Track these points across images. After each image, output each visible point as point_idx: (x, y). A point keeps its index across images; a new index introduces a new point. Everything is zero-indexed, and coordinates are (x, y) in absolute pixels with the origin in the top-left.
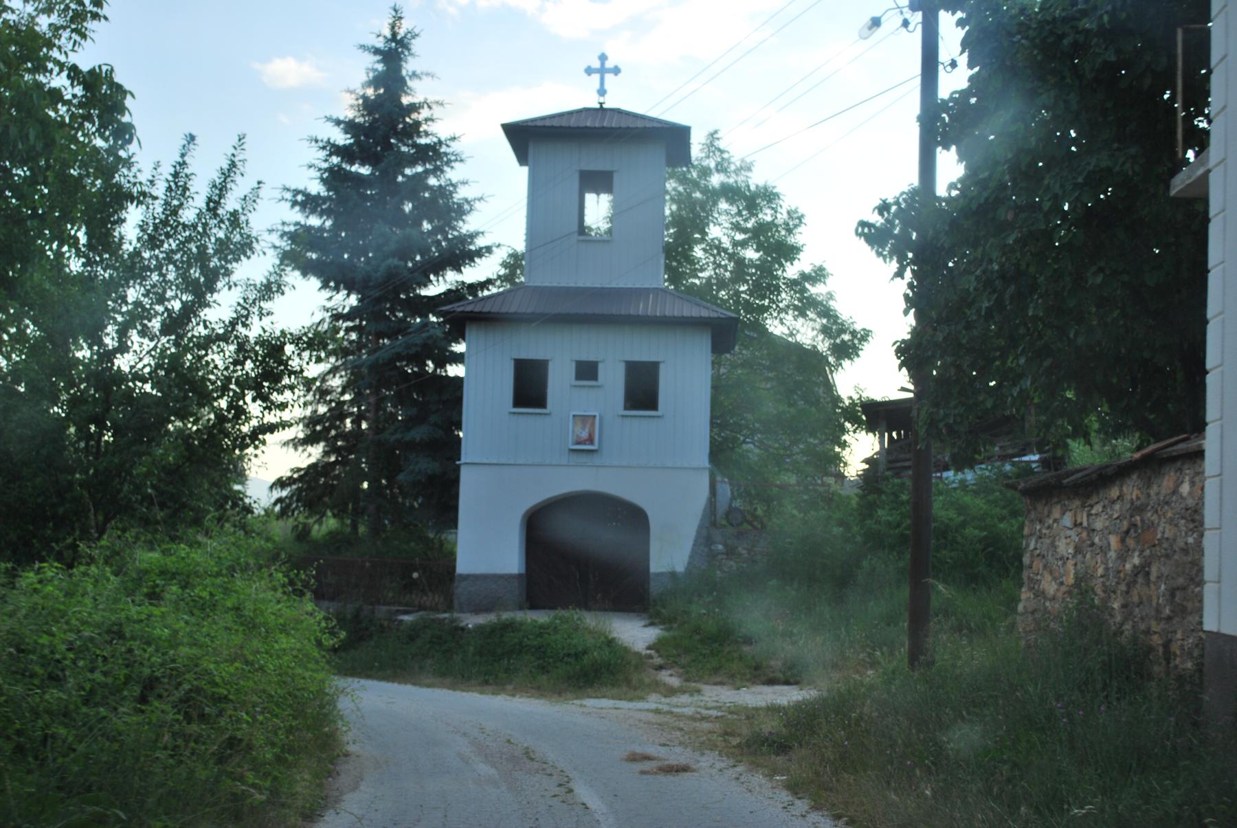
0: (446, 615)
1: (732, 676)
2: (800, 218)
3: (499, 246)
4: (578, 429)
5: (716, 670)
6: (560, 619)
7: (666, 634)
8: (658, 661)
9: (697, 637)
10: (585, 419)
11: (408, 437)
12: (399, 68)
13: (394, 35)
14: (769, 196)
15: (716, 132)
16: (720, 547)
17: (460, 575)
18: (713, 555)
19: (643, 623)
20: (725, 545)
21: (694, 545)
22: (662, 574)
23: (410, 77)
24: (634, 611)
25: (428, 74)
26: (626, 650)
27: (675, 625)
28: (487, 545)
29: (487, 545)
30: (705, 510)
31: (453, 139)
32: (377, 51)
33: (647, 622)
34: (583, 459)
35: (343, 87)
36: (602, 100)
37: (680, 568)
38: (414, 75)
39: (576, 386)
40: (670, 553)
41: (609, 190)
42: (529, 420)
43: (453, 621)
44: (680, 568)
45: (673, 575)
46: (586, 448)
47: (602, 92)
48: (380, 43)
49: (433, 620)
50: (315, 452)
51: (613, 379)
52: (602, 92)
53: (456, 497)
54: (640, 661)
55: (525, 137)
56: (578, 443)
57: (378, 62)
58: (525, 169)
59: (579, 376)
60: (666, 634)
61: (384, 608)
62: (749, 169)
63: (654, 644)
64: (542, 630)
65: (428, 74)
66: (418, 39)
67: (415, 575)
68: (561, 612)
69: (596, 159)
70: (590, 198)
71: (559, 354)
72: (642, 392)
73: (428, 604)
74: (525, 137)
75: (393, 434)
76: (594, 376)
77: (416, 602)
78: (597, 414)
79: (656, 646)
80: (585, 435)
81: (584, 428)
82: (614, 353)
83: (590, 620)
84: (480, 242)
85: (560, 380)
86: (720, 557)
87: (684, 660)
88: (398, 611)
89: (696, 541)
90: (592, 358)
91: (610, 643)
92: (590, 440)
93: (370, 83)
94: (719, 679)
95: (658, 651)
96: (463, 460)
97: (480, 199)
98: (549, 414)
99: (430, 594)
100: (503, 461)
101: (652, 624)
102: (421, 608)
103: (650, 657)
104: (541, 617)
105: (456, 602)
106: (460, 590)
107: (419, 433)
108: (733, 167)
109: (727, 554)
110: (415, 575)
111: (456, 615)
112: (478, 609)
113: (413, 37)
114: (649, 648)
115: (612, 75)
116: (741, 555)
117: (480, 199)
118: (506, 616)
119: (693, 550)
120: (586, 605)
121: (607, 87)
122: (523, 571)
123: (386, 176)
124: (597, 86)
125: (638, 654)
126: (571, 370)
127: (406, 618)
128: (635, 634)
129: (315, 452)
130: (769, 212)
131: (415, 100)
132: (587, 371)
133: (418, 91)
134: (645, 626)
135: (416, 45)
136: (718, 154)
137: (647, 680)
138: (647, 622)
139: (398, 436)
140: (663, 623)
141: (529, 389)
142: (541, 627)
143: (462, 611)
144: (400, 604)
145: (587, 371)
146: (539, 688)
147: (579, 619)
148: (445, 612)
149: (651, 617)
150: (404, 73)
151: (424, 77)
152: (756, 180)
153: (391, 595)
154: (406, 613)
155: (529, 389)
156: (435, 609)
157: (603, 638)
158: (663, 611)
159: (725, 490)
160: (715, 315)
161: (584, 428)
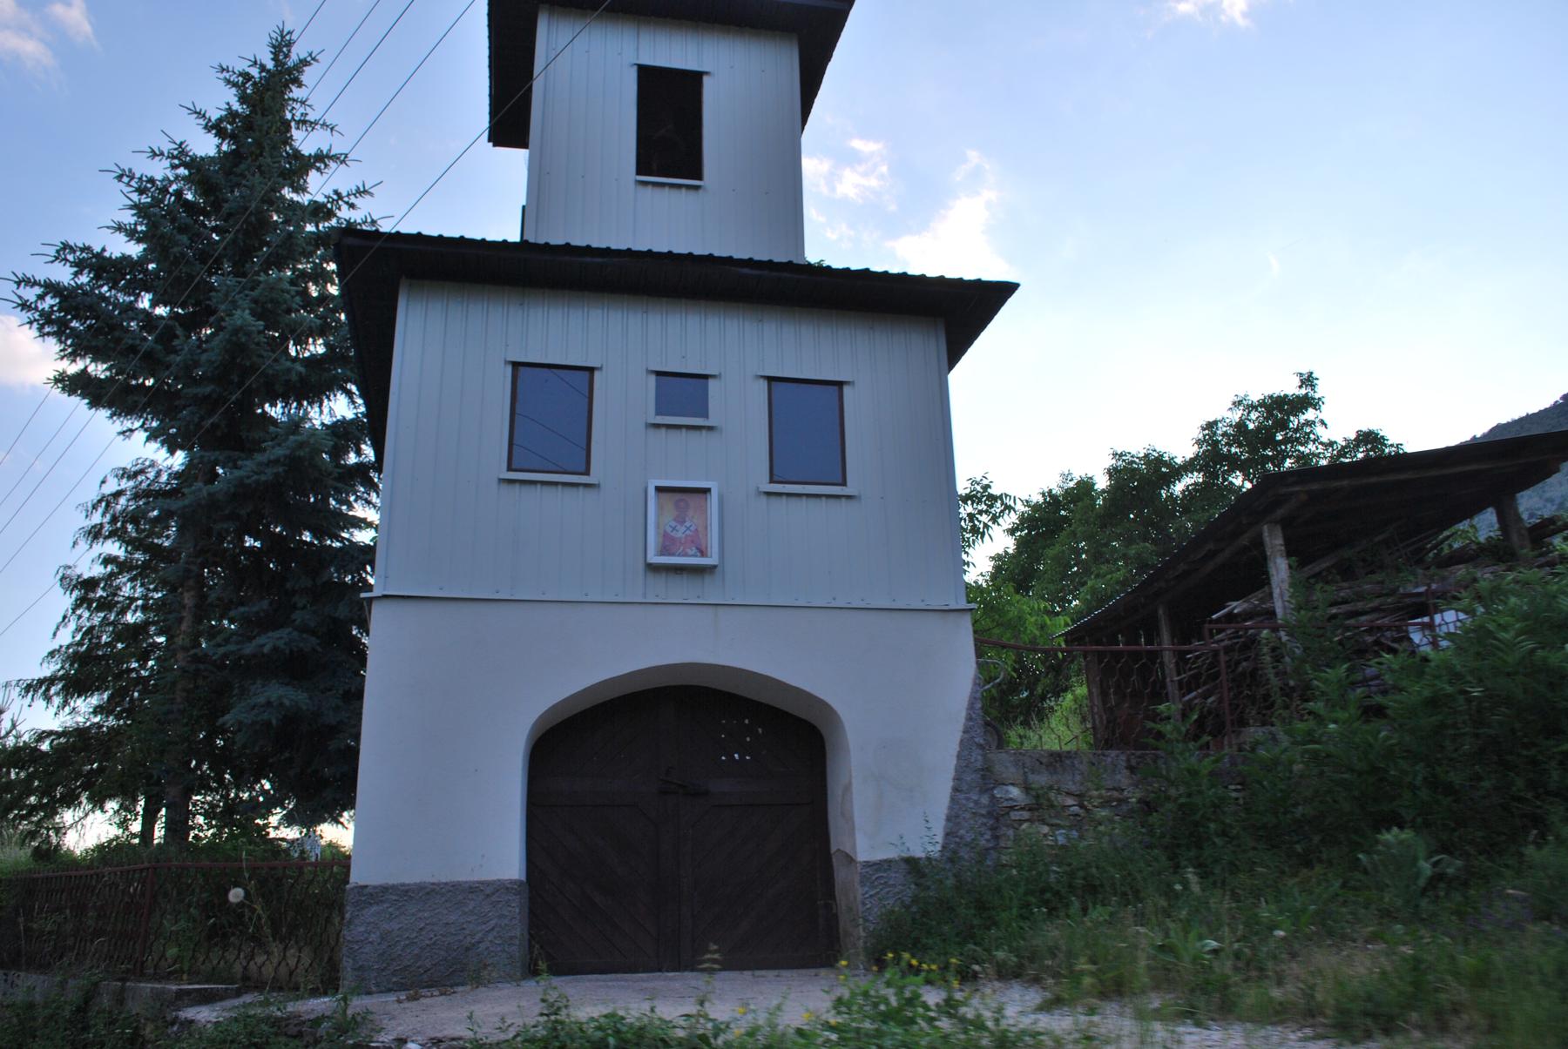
0: (321, 1005)
16: (1015, 792)
18: (998, 815)
20: (1027, 789)
21: (956, 789)
23: (298, 122)
25: (324, 125)
30: (971, 707)
31: (361, 192)
34: (680, 589)
35: (181, 120)
39: (657, 426)
42: (549, 508)
49: (275, 1022)
50: (83, 710)
51: (740, 407)
53: (360, 719)
73: (268, 971)
77: (238, 968)
85: (623, 402)
88: (180, 994)
99: (276, 948)
102: (250, 983)
105: (347, 964)
106: (361, 932)
110: (236, 895)
111: (358, 1004)
122: (523, 878)
127: (204, 1015)
129: (83, 710)
132: (682, 393)
135: (308, 76)
139: (232, 647)
144: (194, 975)
148: (315, 993)
153: (172, 952)
154: (206, 998)
156: (290, 986)
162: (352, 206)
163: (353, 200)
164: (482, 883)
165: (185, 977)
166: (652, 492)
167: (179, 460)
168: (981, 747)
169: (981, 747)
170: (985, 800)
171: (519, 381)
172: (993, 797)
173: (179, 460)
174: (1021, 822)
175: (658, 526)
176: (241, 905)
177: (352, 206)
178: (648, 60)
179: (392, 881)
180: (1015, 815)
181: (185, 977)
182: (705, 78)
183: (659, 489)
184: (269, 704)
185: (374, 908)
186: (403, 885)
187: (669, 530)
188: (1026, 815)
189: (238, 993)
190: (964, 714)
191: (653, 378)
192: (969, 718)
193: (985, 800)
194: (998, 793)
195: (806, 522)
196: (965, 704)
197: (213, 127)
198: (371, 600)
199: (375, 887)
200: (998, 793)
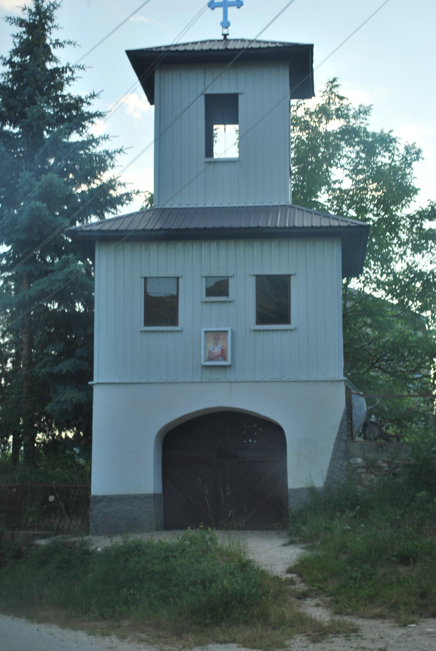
0: (77, 539)
1: (394, 607)
2: (418, 152)
3: (138, 192)
4: (210, 345)
5: (371, 599)
6: (190, 539)
7: (308, 553)
8: (301, 587)
9: (345, 557)
10: (217, 335)
11: (56, 370)
12: (44, 37)
13: (38, 7)
14: (385, 141)
15: (335, 80)
16: (360, 460)
17: (96, 497)
19: (282, 542)
20: (365, 458)
21: (332, 459)
22: (301, 490)
23: (54, 45)
24: (272, 529)
25: (70, 43)
26: (263, 574)
27: (318, 544)
28: (122, 463)
29: (122, 463)
30: (342, 423)
32: (21, 22)
33: (287, 540)
34: (216, 375)
36: (225, 32)
37: (319, 483)
38: (57, 43)
39: (206, 302)
40: (306, 469)
41: (235, 122)
42: (162, 339)
43: (85, 543)
44: (319, 483)
45: (312, 490)
46: (218, 366)
47: (226, 24)
48: (26, 16)
51: (244, 296)
52: (226, 24)
54: (278, 589)
55: (149, 65)
56: (210, 359)
57: (24, 32)
58: (153, 107)
59: (210, 292)
60: (308, 553)
61: (22, 533)
62: (365, 112)
63: (296, 566)
64: (168, 554)
65: (70, 43)
66: (59, 9)
67: (51, 498)
68: (190, 532)
69: (223, 83)
70: (219, 129)
71: (187, 269)
72: (274, 303)
74: (149, 65)
75: (41, 368)
76: (226, 293)
78: (229, 329)
79: (299, 569)
80: (217, 351)
81: (216, 344)
82: (244, 266)
83: (223, 540)
84: (120, 191)
86: (359, 470)
87: (332, 586)
89: (334, 454)
90: (222, 273)
91: (245, 566)
92: (223, 355)
93: (15, 52)
94: (377, 611)
95: (300, 575)
96: (96, 380)
97: (120, 151)
98: (181, 331)
100: (136, 381)
101: (292, 543)
102: (59, 531)
103: (292, 582)
104: (170, 538)
106: (96, 511)
107: (65, 366)
108: (351, 113)
109: (367, 467)
112: (112, 531)
113: (55, 8)
114: (289, 571)
115: (235, 8)
116: (381, 468)
117: (120, 151)
118: (133, 538)
119: (331, 464)
120: (220, 522)
121: (230, 19)
122: (160, 491)
123: (32, 132)
124: (221, 19)
125: (277, 579)
126: (201, 288)
127: (42, 542)
128: (272, 554)
130: (387, 154)
131: (60, 66)
133: (62, 57)
134: (285, 545)
135: (56, 13)
136: (337, 100)
137: (289, 616)
138: (287, 540)
139: (48, 369)
140: (305, 542)
141: (161, 311)
142: (169, 549)
143: (97, 533)
145: (218, 289)
146: (157, 626)
147: (211, 539)
149: (290, 535)
150: (48, 42)
151: (66, 45)
152: (374, 125)
153: (31, 519)
154: (44, 537)
155: (161, 311)
157: (236, 560)
158: (304, 528)
159: (361, 405)
160: (345, 224)
161: (216, 344)
162: (89, 104)
163: (88, 100)
164: (139, 495)
165: (36, 529)
166: (203, 333)
167: (10, 247)
168: (345, 441)
169: (345, 441)
170: (345, 463)
171: (148, 286)
172: (349, 462)
173: (10, 247)
174: (362, 473)
175: (206, 348)
176: (53, 502)
177: (89, 104)
178: (210, 91)
179: (106, 494)
180: (359, 470)
181: (36, 529)
182: (240, 97)
183: (206, 332)
184: (66, 401)
185: (100, 504)
186: (110, 495)
187: (211, 349)
188: (364, 470)
189: (55, 535)
190: (338, 426)
191: (253, 333)
192: (340, 428)
193: (345, 463)
194: (352, 461)
195: (274, 337)
196: (339, 422)
197: (7, 63)
198: (93, 385)
199: (100, 496)
200: (352, 461)
